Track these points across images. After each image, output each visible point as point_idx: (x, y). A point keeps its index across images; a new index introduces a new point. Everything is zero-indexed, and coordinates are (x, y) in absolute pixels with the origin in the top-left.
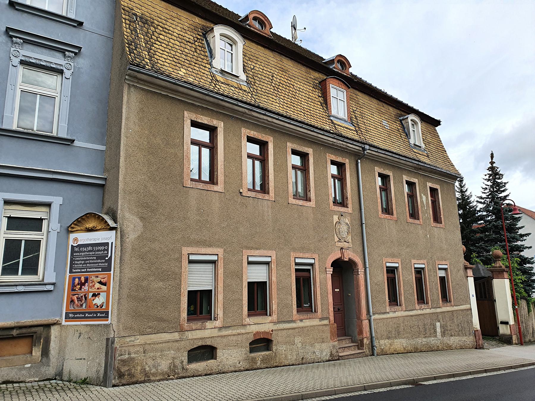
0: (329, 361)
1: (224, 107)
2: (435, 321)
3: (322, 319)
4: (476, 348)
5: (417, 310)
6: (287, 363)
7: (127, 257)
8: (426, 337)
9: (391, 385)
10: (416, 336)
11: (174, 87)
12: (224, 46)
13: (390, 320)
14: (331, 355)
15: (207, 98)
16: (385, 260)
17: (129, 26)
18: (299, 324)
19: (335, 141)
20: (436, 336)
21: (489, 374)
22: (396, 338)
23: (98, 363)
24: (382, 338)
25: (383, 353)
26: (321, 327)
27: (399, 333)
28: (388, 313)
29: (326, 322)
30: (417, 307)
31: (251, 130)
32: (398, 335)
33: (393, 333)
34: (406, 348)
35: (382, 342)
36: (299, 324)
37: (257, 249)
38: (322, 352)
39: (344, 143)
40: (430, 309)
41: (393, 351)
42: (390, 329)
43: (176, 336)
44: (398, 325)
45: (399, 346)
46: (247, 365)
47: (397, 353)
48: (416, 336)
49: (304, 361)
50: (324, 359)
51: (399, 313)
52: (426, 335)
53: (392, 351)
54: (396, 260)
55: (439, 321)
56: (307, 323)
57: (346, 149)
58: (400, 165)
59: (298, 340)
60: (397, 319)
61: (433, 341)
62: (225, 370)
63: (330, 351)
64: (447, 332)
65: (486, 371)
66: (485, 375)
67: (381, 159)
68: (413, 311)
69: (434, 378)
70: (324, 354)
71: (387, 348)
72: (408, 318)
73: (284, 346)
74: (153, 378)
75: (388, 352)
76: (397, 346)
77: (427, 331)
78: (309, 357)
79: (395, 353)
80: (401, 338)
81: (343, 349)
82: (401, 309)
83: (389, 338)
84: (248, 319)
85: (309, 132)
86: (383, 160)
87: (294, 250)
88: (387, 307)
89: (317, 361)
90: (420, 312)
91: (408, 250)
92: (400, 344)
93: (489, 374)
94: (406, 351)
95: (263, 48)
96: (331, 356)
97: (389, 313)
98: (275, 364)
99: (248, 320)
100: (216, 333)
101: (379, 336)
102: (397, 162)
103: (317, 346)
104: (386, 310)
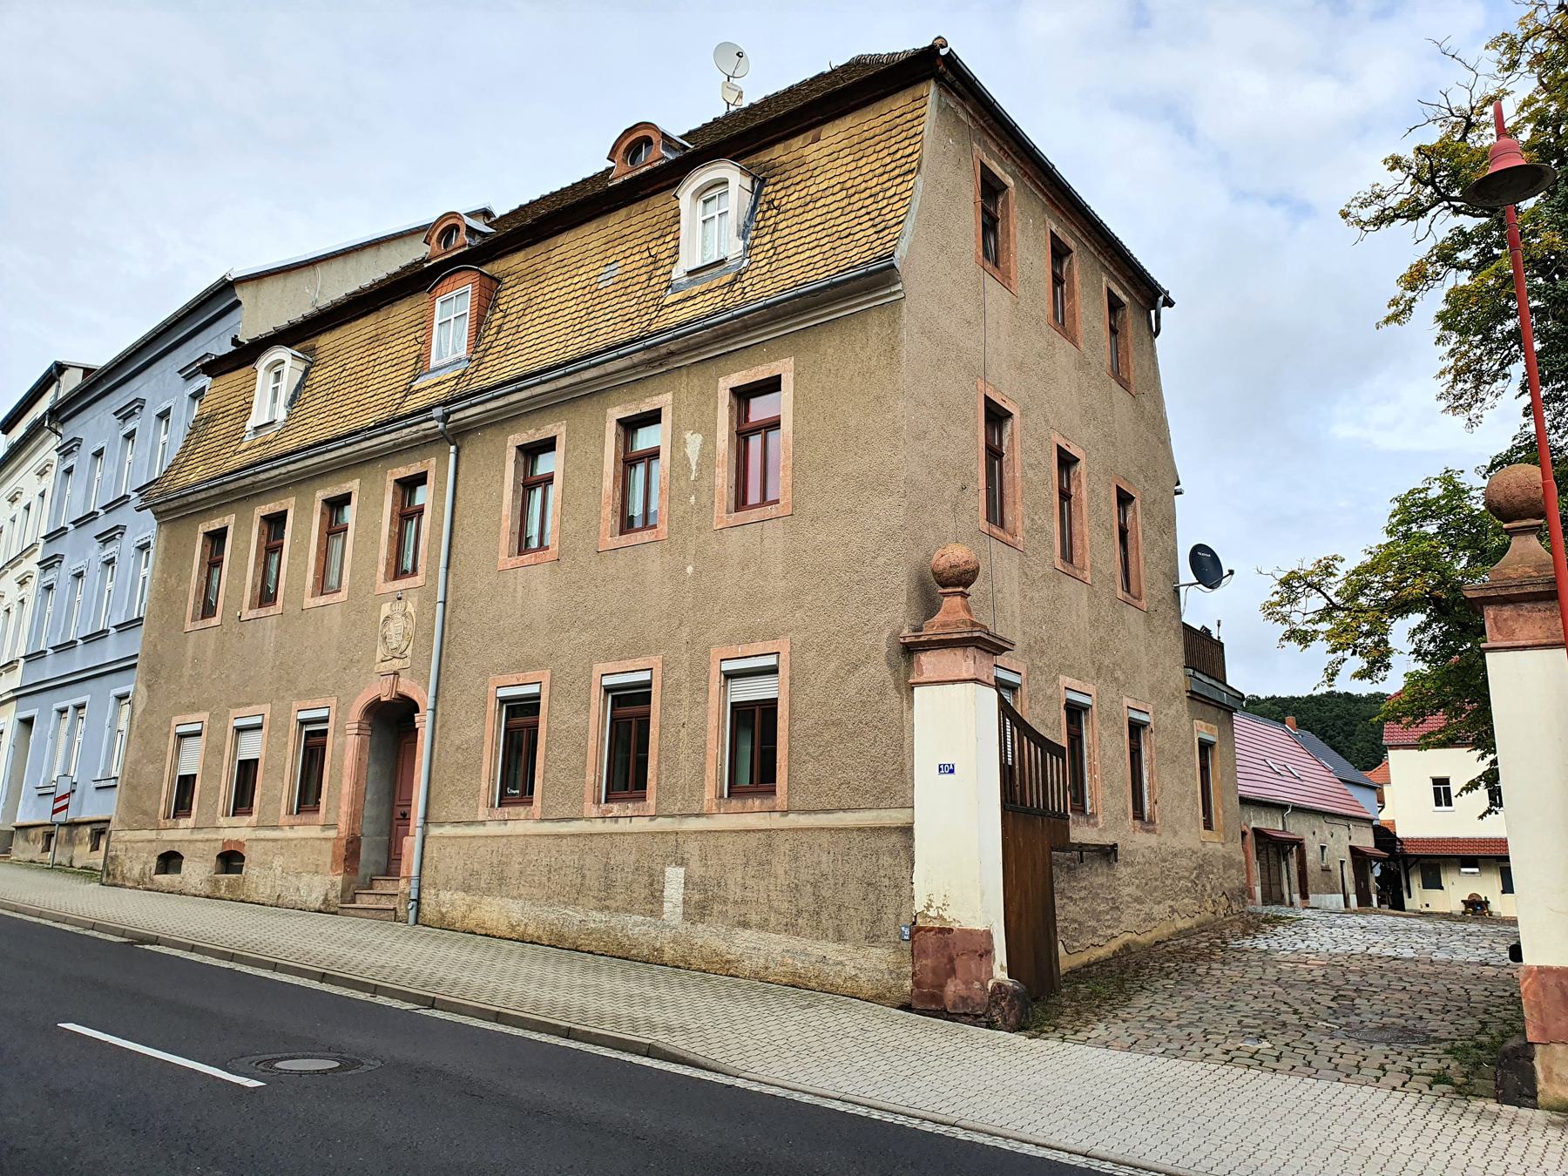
0: (320, 911)
1: (232, 492)
2: (659, 860)
3: (326, 826)
4: (907, 1007)
5: (589, 819)
6: (256, 899)
7: (132, 737)
8: (607, 908)
9: (376, 990)
10: (561, 899)
11: (184, 501)
12: (463, 318)
13: (481, 842)
14: (326, 900)
15: (213, 492)
16: (495, 679)
17: (1553, 29)
18: (288, 833)
19: (393, 436)
20: (656, 913)
21: (325, 987)
22: (488, 891)
23: (440, 911)
24: (447, 886)
25: (444, 925)
26: (318, 842)
27: (502, 880)
28: (483, 823)
29: (332, 834)
30: (594, 812)
31: (265, 504)
32: (500, 883)
33: (484, 877)
34: (519, 925)
35: (445, 896)
36: (288, 833)
37: (249, 704)
38: (311, 891)
39: (414, 429)
40: (653, 817)
41: (471, 926)
42: (476, 867)
43: (152, 835)
44: (504, 859)
45: (495, 916)
46: (207, 889)
47: (486, 935)
48: (561, 899)
49: (280, 901)
50: (311, 906)
51: (521, 824)
52: (607, 903)
53: (470, 924)
54: (531, 675)
55: (682, 862)
56: (300, 832)
57: (426, 436)
58: (597, 385)
59: (278, 862)
60: (504, 840)
61: (635, 927)
62: (186, 891)
63: (324, 893)
64: (717, 907)
65: (275, 967)
66: (315, 985)
67: (523, 407)
68: (571, 824)
69: (195, 949)
70: (314, 896)
71: (457, 914)
72: (546, 841)
73: (258, 869)
74: (127, 884)
75: (457, 925)
76: (488, 914)
77: (619, 891)
78: (290, 897)
79: (478, 931)
80: (507, 896)
81: (378, 897)
82: (527, 815)
83: (467, 889)
84: (222, 819)
85: (345, 451)
86: (531, 405)
87: (299, 696)
88: (480, 808)
89: (300, 906)
90: (599, 826)
91: (585, 637)
92: (500, 913)
93: (325, 987)
94: (514, 935)
95: (364, 319)
96: (324, 903)
97: (484, 825)
98: (242, 897)
99: (222, 821)
100: (187, 835)
101: (440, 880)
102: (571, 385)
103: (306, 878)
104: (476, 814)
